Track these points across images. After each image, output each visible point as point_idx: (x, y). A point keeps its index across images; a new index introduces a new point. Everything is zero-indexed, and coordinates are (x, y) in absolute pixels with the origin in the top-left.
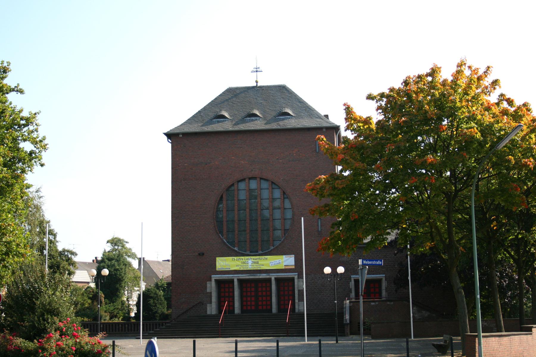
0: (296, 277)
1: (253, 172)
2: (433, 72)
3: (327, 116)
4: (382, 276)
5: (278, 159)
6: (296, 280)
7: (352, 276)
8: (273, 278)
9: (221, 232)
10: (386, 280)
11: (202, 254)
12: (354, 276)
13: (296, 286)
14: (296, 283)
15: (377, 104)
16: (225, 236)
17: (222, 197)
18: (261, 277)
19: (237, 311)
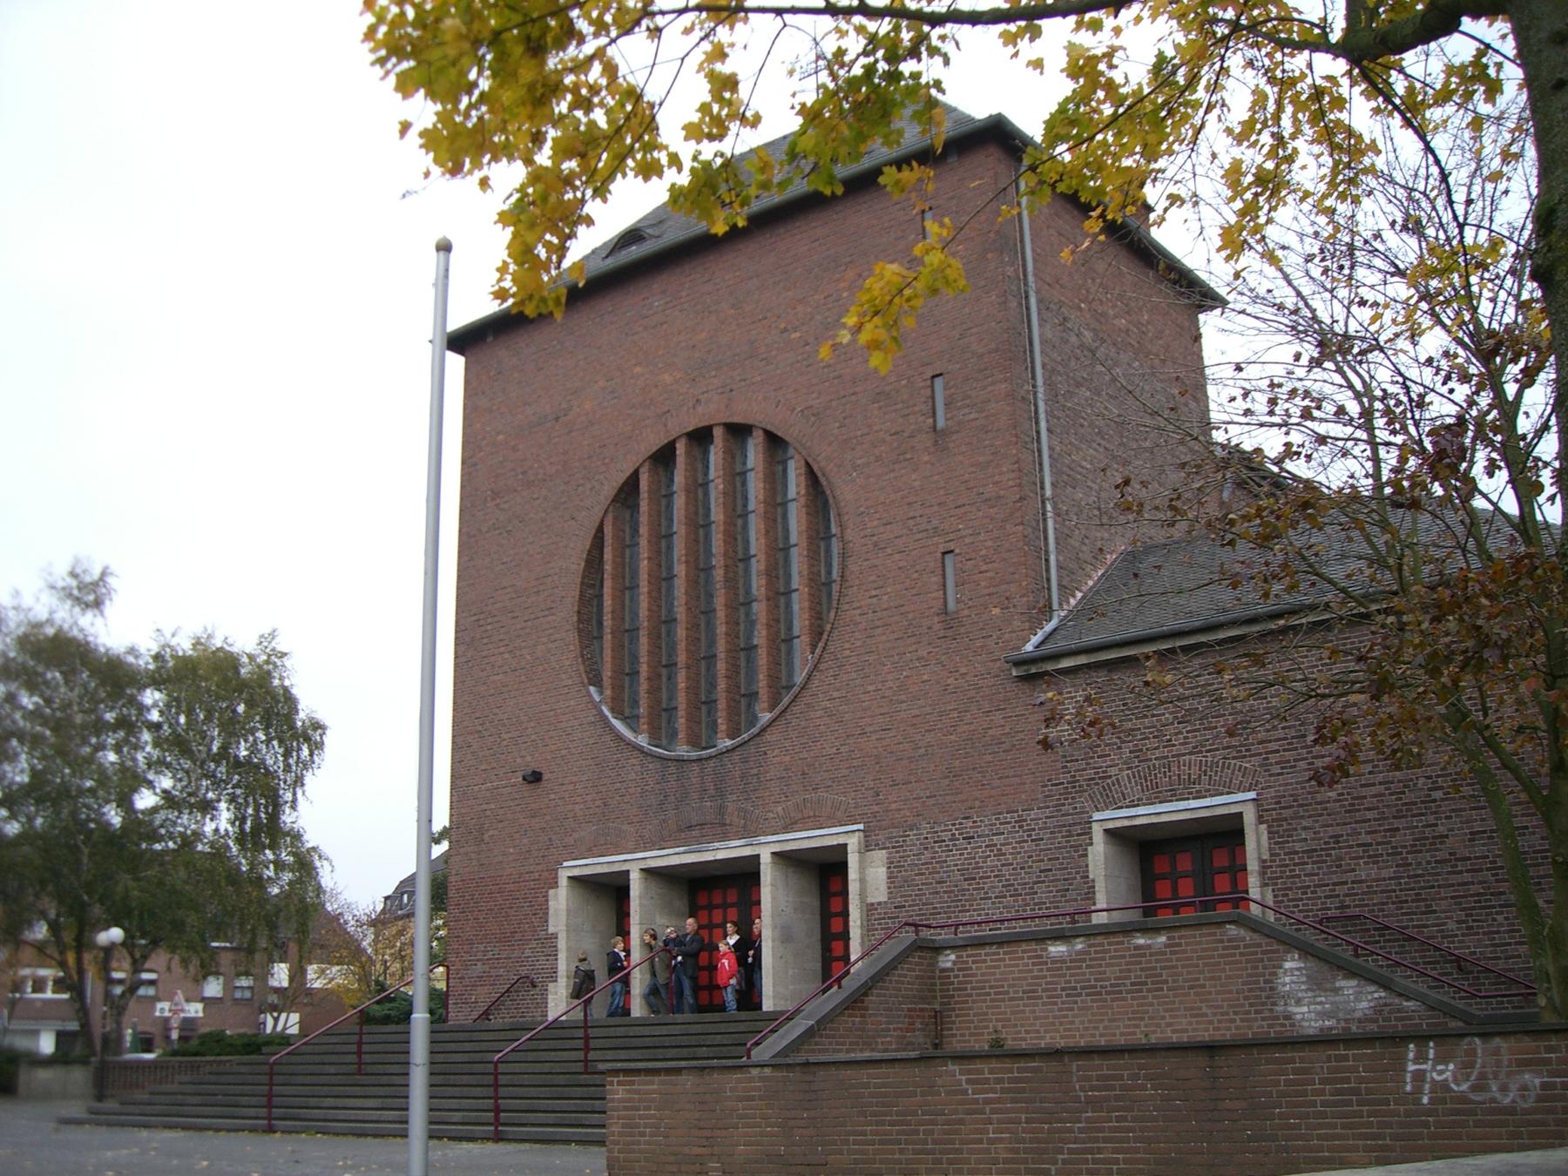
0: (853, 843)
1: (700, 409)
2: (210, 637)
3: (387, 898)
4: (1238, 801)
5: (785, 330)
6: (853, 860)
7: (1097, 816)
8: (766, 859)
9: (596, 681)
10: (1260, 820)
11: (535, 778)
12: (1107, 814)
13: (853, 888)
14: (853, 874)
15: (631, 174)
16: (608, 692)
17: (600, 529)
18: (721, 855)
19: (638, 1009)
